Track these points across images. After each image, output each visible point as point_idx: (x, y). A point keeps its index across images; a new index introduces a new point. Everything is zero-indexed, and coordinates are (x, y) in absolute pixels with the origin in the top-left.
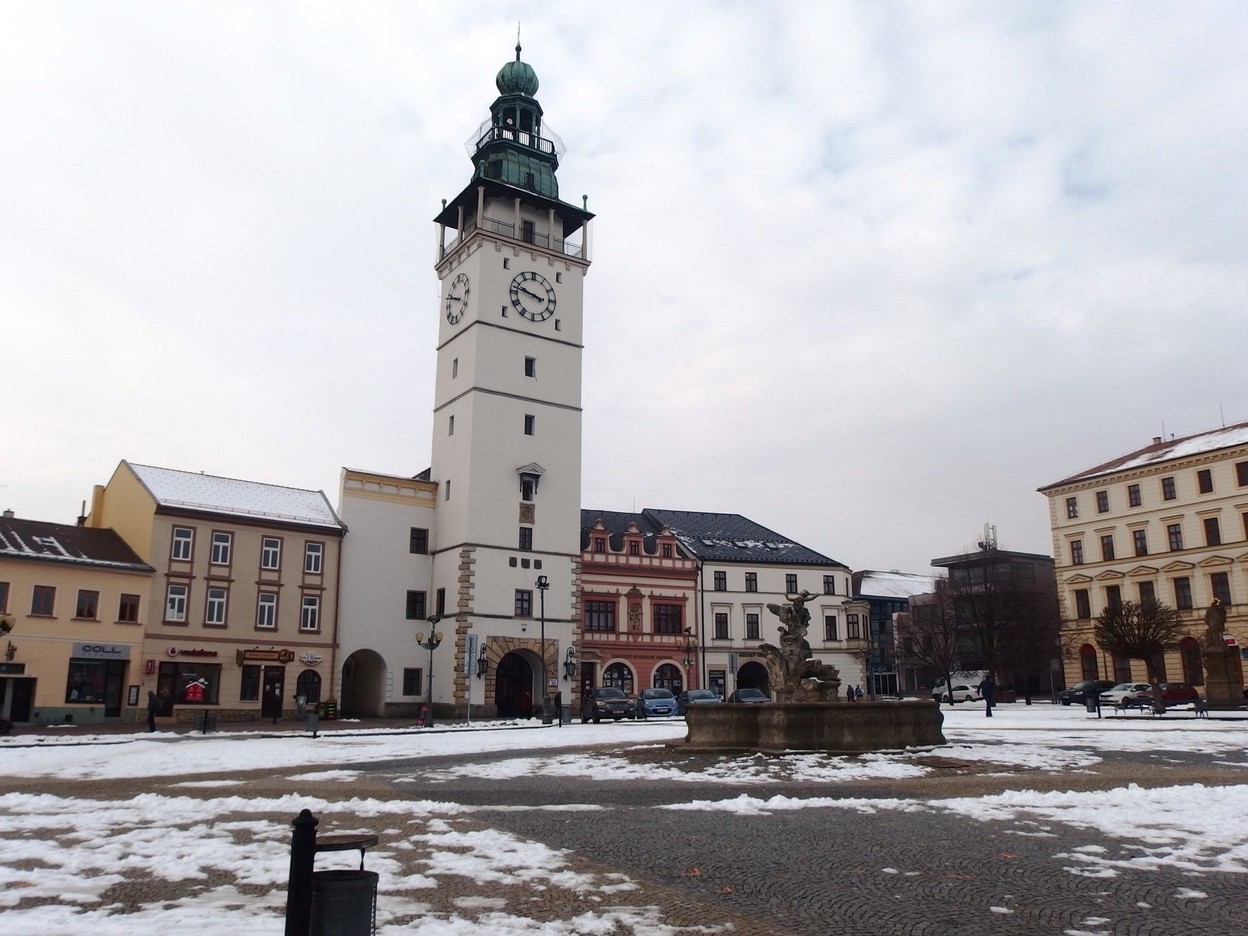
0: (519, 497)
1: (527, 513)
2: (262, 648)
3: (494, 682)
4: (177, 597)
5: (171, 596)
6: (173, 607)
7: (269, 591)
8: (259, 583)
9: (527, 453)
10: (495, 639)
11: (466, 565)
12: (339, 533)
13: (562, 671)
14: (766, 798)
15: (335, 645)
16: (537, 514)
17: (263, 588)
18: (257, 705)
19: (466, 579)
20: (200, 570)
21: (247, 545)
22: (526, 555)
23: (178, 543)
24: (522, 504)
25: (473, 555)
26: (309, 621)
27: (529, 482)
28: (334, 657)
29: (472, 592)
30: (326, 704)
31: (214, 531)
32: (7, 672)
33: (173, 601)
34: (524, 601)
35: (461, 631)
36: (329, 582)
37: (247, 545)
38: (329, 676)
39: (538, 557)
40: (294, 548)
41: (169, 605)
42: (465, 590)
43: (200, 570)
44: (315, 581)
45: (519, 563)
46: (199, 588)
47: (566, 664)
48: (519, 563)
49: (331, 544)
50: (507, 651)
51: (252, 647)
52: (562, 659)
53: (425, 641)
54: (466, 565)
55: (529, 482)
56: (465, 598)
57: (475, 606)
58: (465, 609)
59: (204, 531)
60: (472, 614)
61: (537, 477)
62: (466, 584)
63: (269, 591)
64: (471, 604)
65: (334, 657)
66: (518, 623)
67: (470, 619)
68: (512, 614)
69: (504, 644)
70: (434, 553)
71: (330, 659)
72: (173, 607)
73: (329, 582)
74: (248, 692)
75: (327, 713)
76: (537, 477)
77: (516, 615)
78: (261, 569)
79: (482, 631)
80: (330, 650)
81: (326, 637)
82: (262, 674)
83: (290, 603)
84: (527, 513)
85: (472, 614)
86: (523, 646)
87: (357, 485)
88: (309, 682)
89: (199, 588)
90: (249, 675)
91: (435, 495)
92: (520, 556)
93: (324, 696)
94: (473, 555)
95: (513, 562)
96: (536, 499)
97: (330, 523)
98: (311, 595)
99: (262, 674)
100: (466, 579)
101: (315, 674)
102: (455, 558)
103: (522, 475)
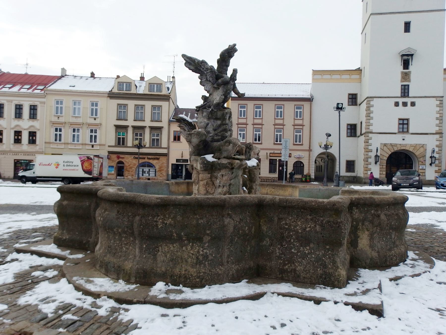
0: (400, 68)
1: (406, 76)
2: (276, 152)
3: (385, 167)
4: (242, 133)
5: (239, 132)
6: (241, 137)
7: (279, 128)
8: (274, 125)
9: (405, 43)
10: (385, 145)
11: (369, 108)
12: (310, 100)
13: (428, 161)
14: (122, 304)
15: (310, 150)
16: (412, 76)
17: (276, 127)
18: (276, 175)
19: (368, 116)
20: (250, 121)
21: (269, 110)
22: (405, 100)
23: (241, 111)
24: (402, 73)
25: (372, 103)
26: (298, 140)
27: (406, 60)
28: (309, 155)
29: (371, 121)
30: (306, 176)
31: (255, 105)
32: (182, 162)
33: (240, 134)
34: (404, 124)
35: (366, 142)
36: (306, 122)
37: (269, 110)
38: (308, 163)
39: (413, 100)
40: (289, 108)
41: (239, 136)
42: (368, 121)
43: (250, 121)
44: (300, 122)
45: (401, 104)
46: (250, 128)
47: (431, 157)
48: (401, 104)
49: (306, 105)
50: (393, 151)
51: (272, 152)
52: (429, 154)
53: (323, 146)
54: (369, 108)
55: (406, 60)
56: (369, 125)
57: (373, 129)
58: (368, 130)
59: (289, 108)
60: (371, 133)
61: (412, 55)
62: (369, 118)
63: (279, 128)
64: (371, 128)
65: (309, 155)
66: (401, 136)
67: (370, 135)
68: (396, 131)
69: (391, 147)
70: (360, 105)
71: (308, 156)
72: (241, 137)
73: (306, 122)
74: (272, 170)
75: (306, 180)
76: (412, 55)
77: (399, 132)
78: (254, 118)
79: (377, 142)
80: (308, 153)
81: (306, 146)
82: (278, 162)
83: (289, 133)
84: (406, 76)
85: (371, 133)
86: (403, 148)
87: (319, 77)
88: (299, 166)
89: (250, 128)
90: (272, 163)
91: (361, 76)
92: (401, 101)
93: (306, 172)
94: (372, 103)
95: (397, 104)
96: (412, 68)
97: (307, 95)
98: (298, 128)
99: (278, 162)
100: (368, 116)
101: (301, 163)
102: (364, 106)
103: (403, 55)
